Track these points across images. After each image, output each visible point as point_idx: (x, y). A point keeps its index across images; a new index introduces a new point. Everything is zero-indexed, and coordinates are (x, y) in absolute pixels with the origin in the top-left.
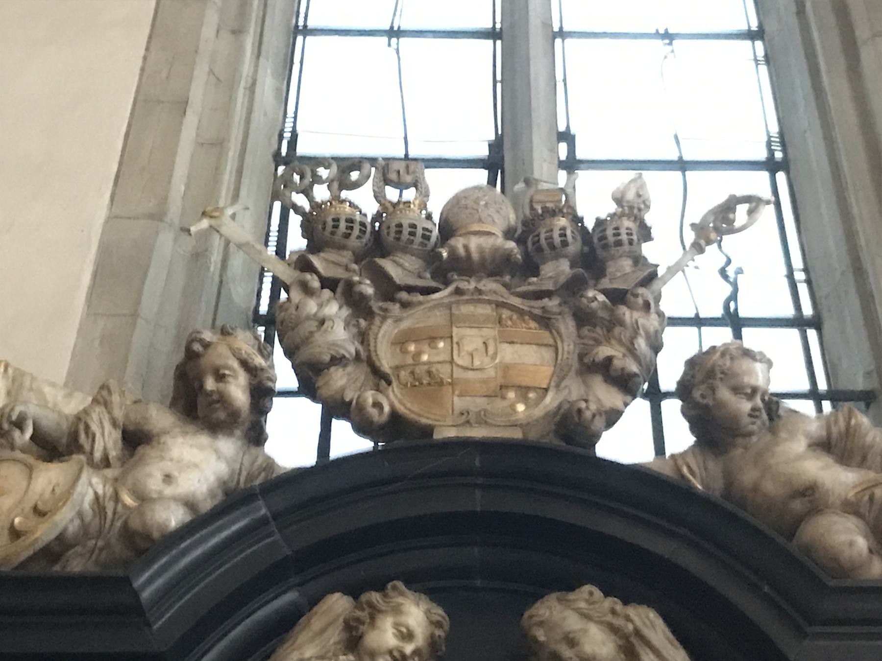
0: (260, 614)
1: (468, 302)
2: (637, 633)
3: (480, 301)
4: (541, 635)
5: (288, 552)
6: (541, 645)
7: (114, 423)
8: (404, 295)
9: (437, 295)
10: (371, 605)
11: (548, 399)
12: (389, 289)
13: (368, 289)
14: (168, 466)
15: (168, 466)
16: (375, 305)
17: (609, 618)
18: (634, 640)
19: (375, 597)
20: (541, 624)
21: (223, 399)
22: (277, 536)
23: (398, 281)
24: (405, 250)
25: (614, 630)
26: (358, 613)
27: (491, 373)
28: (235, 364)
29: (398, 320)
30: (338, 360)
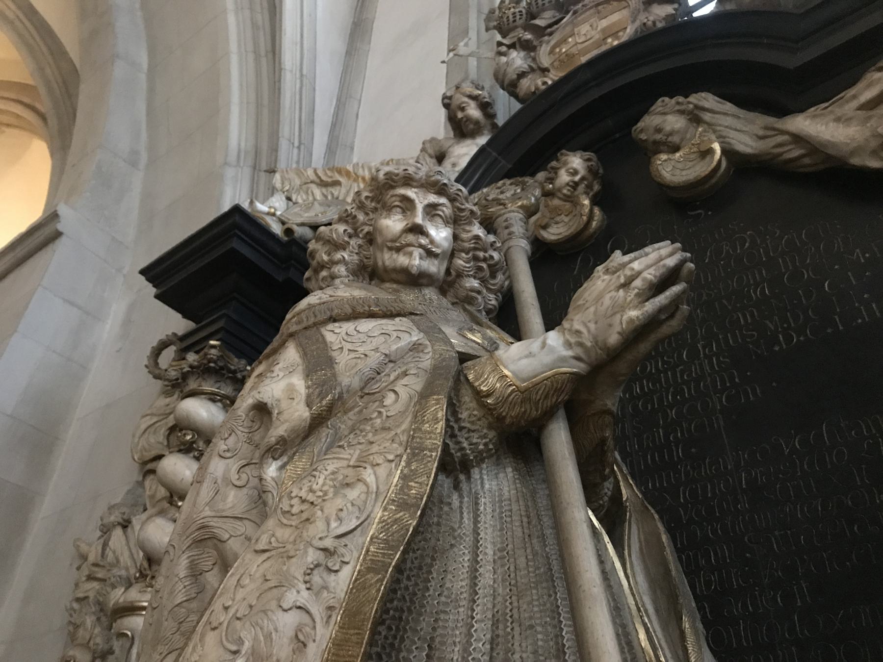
0: (234, 59)
1: (581, 14)
2: (697, 107)
3: (586, 11)
4: (643, 136)
5: (510, 166)
6: (646, 140)
7: (431, 157)
8: (549, 30)
9: (565, 20)
10: (552, 168)
11: (628, 30)
12: (540, 32)
13: (528, 36)
14: (452, 160)
15: (452, 160)
16: (535, 43)
17: (678, 107)
18: (696, 112)
19: (554, 164)
20: (642, 131)
21: (468, 119)
22: (503, 162)
23: (543, 25)
24: (544, 10)
25: (681, 112)
26: (550, 175)
27: (597, 37)
28: (466, 99)
29: (548, 42)
30: (522, 75)
